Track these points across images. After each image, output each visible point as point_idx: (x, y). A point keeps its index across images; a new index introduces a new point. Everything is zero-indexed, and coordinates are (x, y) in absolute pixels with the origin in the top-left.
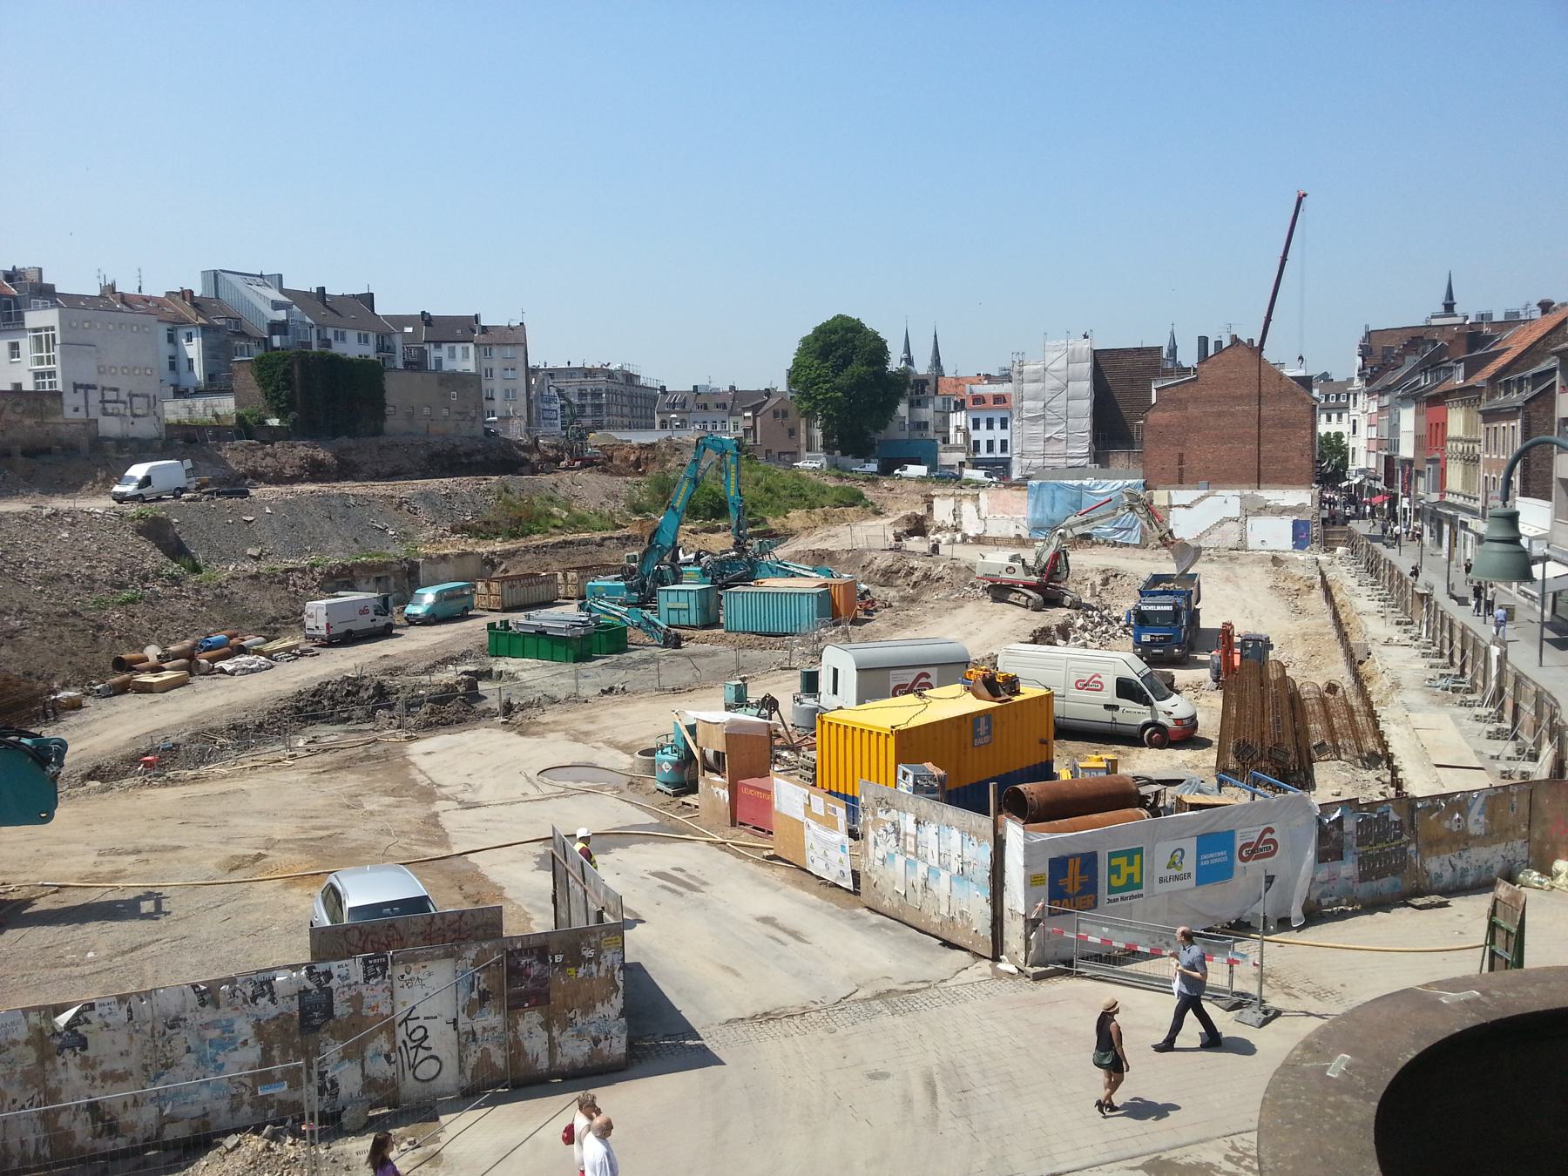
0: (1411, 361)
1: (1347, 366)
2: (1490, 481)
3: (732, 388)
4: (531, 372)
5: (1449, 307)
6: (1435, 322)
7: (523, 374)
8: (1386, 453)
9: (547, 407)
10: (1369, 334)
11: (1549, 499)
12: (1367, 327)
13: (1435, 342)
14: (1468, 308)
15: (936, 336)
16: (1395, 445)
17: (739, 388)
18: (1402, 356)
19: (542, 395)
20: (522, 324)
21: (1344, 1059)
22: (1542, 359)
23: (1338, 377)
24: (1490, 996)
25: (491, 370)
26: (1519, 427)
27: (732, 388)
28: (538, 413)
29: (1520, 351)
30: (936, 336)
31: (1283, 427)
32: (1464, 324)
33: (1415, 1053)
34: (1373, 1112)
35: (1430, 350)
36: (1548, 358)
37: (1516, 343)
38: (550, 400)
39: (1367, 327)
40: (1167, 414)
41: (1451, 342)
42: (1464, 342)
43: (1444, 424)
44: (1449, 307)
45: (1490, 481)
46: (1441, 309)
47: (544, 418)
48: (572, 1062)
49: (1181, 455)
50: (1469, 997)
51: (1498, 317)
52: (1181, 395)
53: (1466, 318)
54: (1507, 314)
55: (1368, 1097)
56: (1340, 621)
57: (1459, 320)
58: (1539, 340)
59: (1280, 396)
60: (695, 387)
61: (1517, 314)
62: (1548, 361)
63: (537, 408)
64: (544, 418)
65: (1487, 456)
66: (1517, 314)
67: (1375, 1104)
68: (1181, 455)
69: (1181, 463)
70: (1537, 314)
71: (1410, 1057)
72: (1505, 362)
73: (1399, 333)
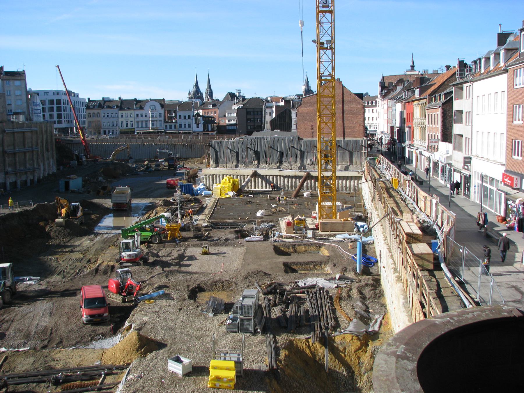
0: (399, 88)
1: (375, 90)
2: (430, 135)
3: (120, 98)
4: (28, 92)
5: (413, 67)
6: (408, 73)
7: (25, 93)
8: (391, 125)
9: (36, 108)
10: (383, 77)
11: (451, 142)
12: (382, 75)
13: (408, 81)
14: (420, 69)
15: (209, 76)
16: (393, 121)
17: (124, 98)
18: (396, 86)
19: (34, 102)
20: (24, 71)
21: (403, 347)
22: (447, 88)
23: (372, 94)
24: (453, 319)
25: (10, 91)
26: (440, 114)
27: (120, 98)
28: (32, 111)
29: (439, 84)
30: (209, 76)
31: (352, 114)
32: (418, 74)
33: (428, 342)
34: (416, 365)
35: (406, 84)
36: (449, 88)
37: (438, 82)
38: (37, 105)
39: (382, 75)
40: (306, 109)
41: (414, 81)
42: (419, 81)
43: (413, 113)
44: (413, 67)
45: (430, 135)
46: (410, 68)
47: (35, 113)
48: (45, 261)
49: (312, 126)
50: (446, 320)
51: (431, 72)
52: (311, 101)
53: (419, 72)
54: (433, 71)
55: (413, 361)
56: (440, 88)
57: (416, 73)
58: (446, 80)
59: (350, 102)
60: (103, 98)
61: (437, 71)
62: (449, 89)
63: (32, 108)
64: (35, 113)
65: (428, 126)
66: (437, 71)
67: (416, 363)
68: (312, 126)
69: (312, 129)
70: (445, 71)
71: (427, 344)
72: (434, 89)
73: (394, 77)
